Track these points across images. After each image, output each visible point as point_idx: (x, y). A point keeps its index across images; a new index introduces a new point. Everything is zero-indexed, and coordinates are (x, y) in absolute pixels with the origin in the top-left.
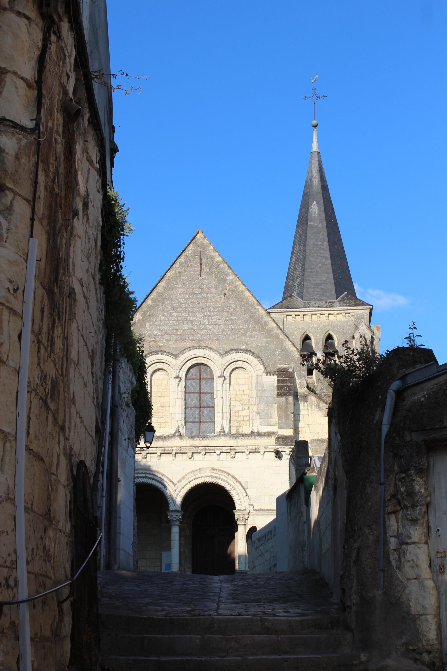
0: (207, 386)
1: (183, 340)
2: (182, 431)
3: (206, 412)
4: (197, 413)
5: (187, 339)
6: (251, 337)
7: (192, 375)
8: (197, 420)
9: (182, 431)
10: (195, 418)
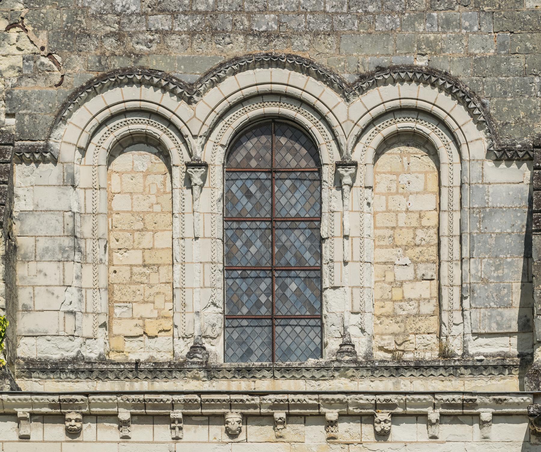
0: (298, 195)
1: (214, 32)
2: (216, 349)
3: (293, 287)
4: (263, 286)
5: (229, 27)
6: (447, 23)
7: (248, 157)
8: (264, 311)
9: (216, 349)
10: (258, 304)
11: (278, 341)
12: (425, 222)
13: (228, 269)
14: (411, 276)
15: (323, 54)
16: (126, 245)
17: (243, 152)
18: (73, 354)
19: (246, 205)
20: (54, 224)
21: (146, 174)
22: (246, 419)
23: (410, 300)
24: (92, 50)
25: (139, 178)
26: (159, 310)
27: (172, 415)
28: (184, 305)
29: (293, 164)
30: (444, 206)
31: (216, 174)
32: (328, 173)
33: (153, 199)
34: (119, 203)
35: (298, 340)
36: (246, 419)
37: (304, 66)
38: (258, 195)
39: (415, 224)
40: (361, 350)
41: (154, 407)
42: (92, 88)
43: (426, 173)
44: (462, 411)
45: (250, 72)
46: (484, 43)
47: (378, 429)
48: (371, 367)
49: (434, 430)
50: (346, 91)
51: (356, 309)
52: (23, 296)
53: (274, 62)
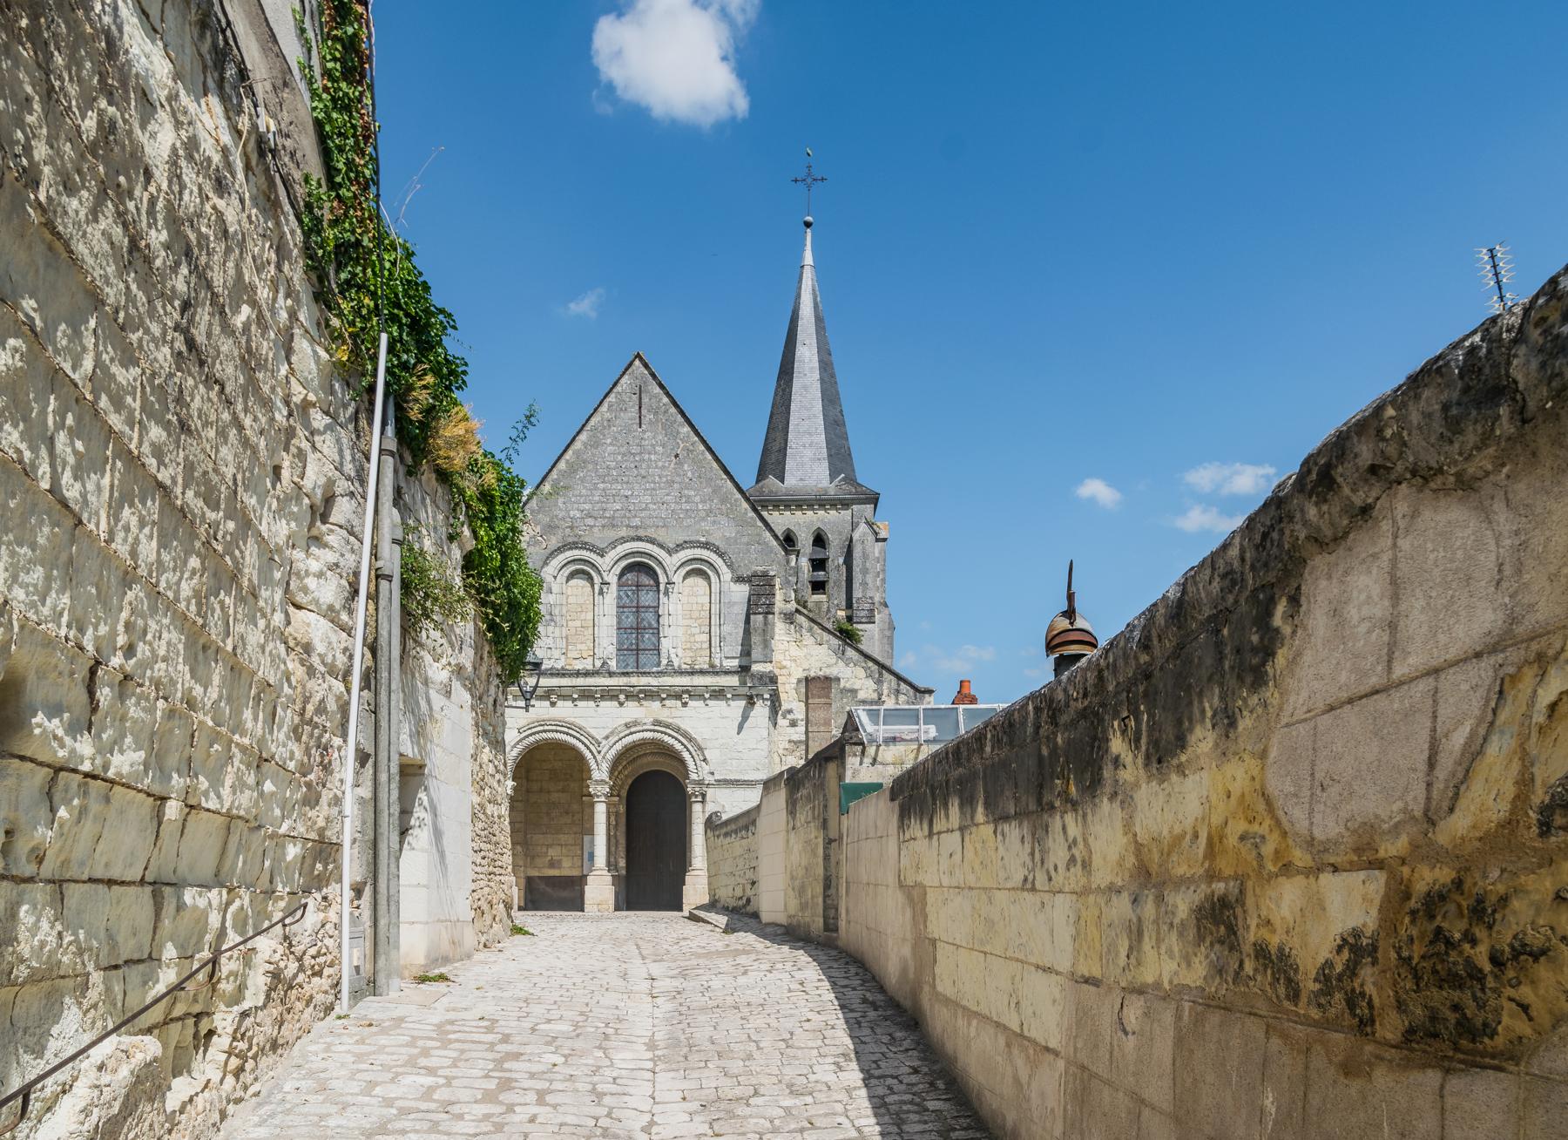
2: (613, 664)
9: (613, 664)
15: (661, 535)
19: (626, 601)
31: (614, 587)
32: (662, 587)
34: (571, 600)
37: (652, 541)
40: (676, 665)
42: (559, 550)
44: (718, 694)
46: (731, 532)
48: (681, 673)
50: (670, 552)
53: (639, 539)
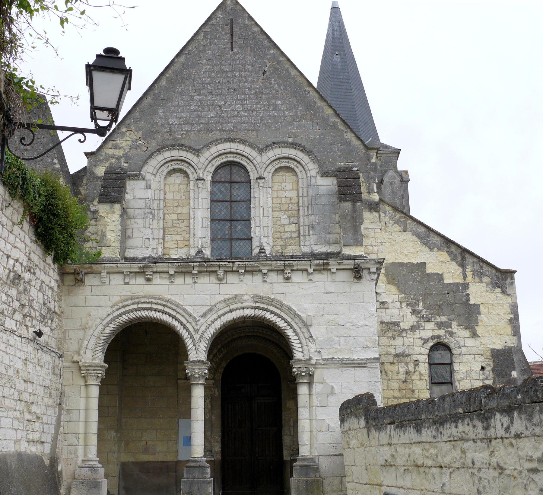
0: (241, 191)
3: (239, 227)
4: (227, 227)
7: (221, 177)
8: (227, 237)
9: (207, 253)
10: (225, 234)
11: (233, 249)
12: (293, 201)
13: (212, 220)
14: (288, 222)
15: (252, 137)
16: (170, 212)
17: (219, 176)
18: (148, 255)
20: (142, 204)
21: (179, 185)
22: (226, 272)
23: (287, 232)
24: (159, 137)
25: (177, 186)
26: (184, 237)
27: (193, 272)
28: (194, 235)
29: (239, 180)
30: (300, 195)
33: (182, 194)
35: (241, 248)
36: (226, 272)
38: (225, 192)
39: (289, 202)
41: (185, 267)
42: (158, 151)
43: (292, 182)
45: (222, 145)
47: (286, 277)
49: (311, 277)
50: (261, 151)
51: (266, 235)
52: (129, 232)
53: (232, 140)
